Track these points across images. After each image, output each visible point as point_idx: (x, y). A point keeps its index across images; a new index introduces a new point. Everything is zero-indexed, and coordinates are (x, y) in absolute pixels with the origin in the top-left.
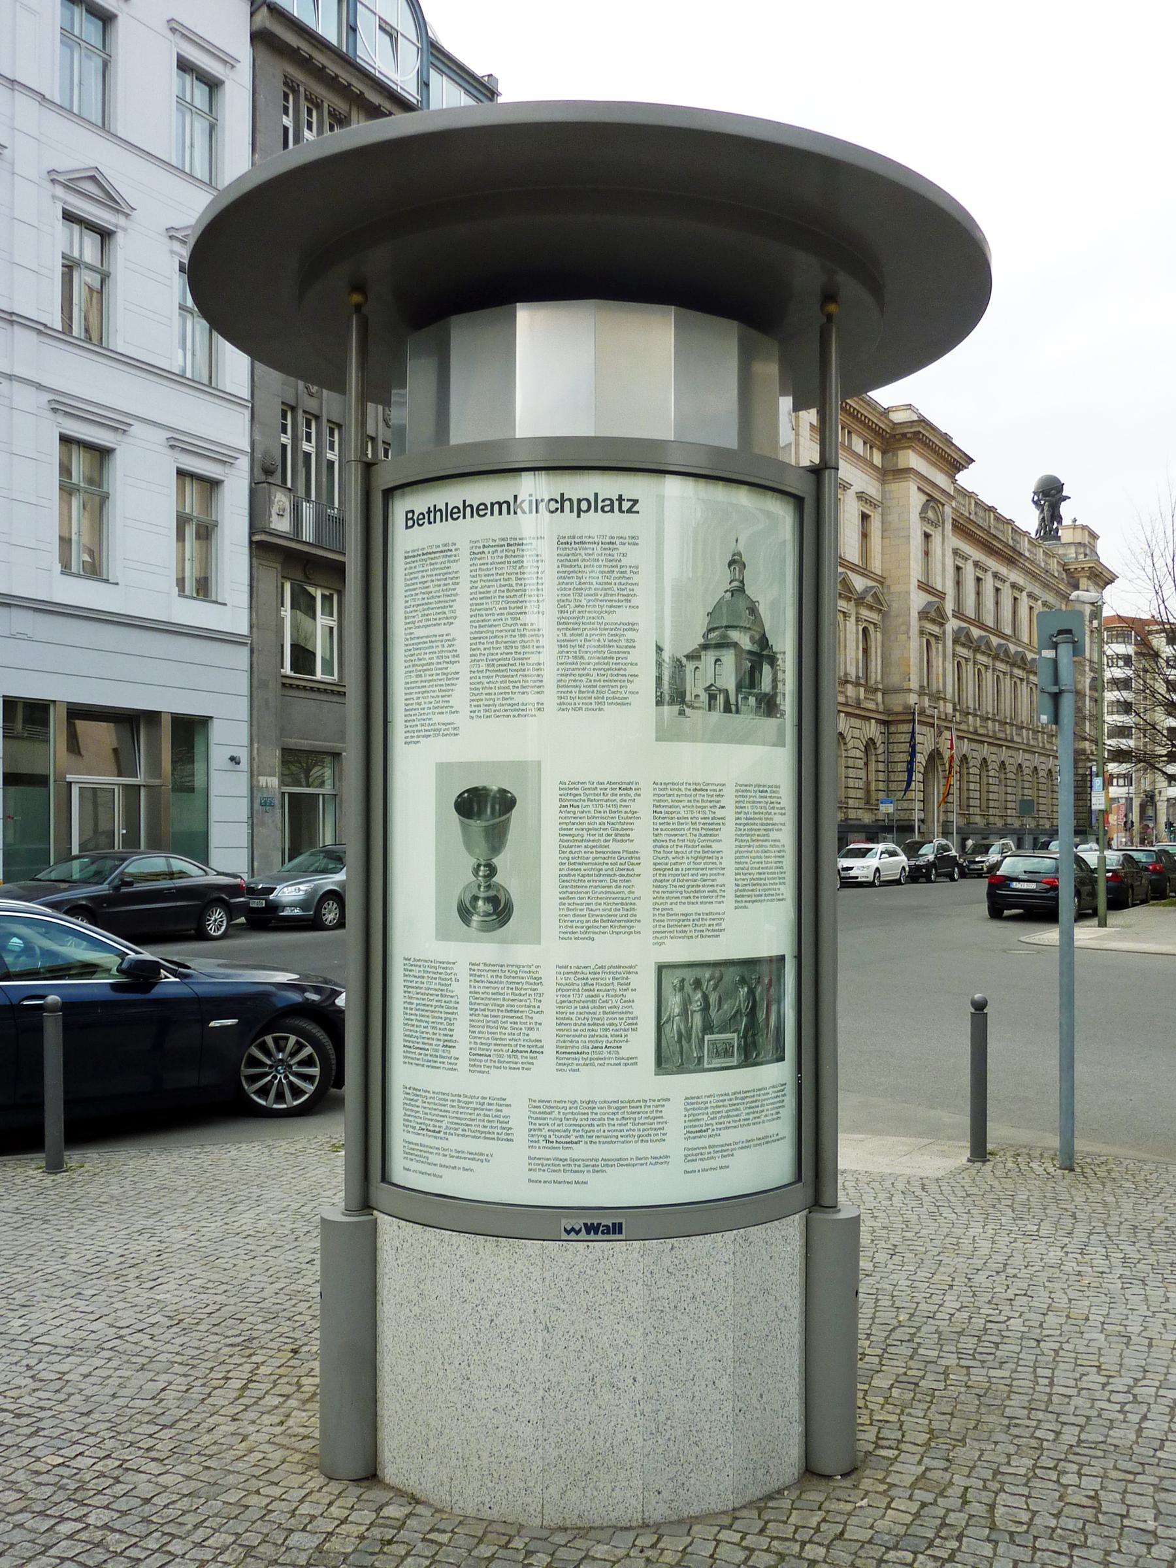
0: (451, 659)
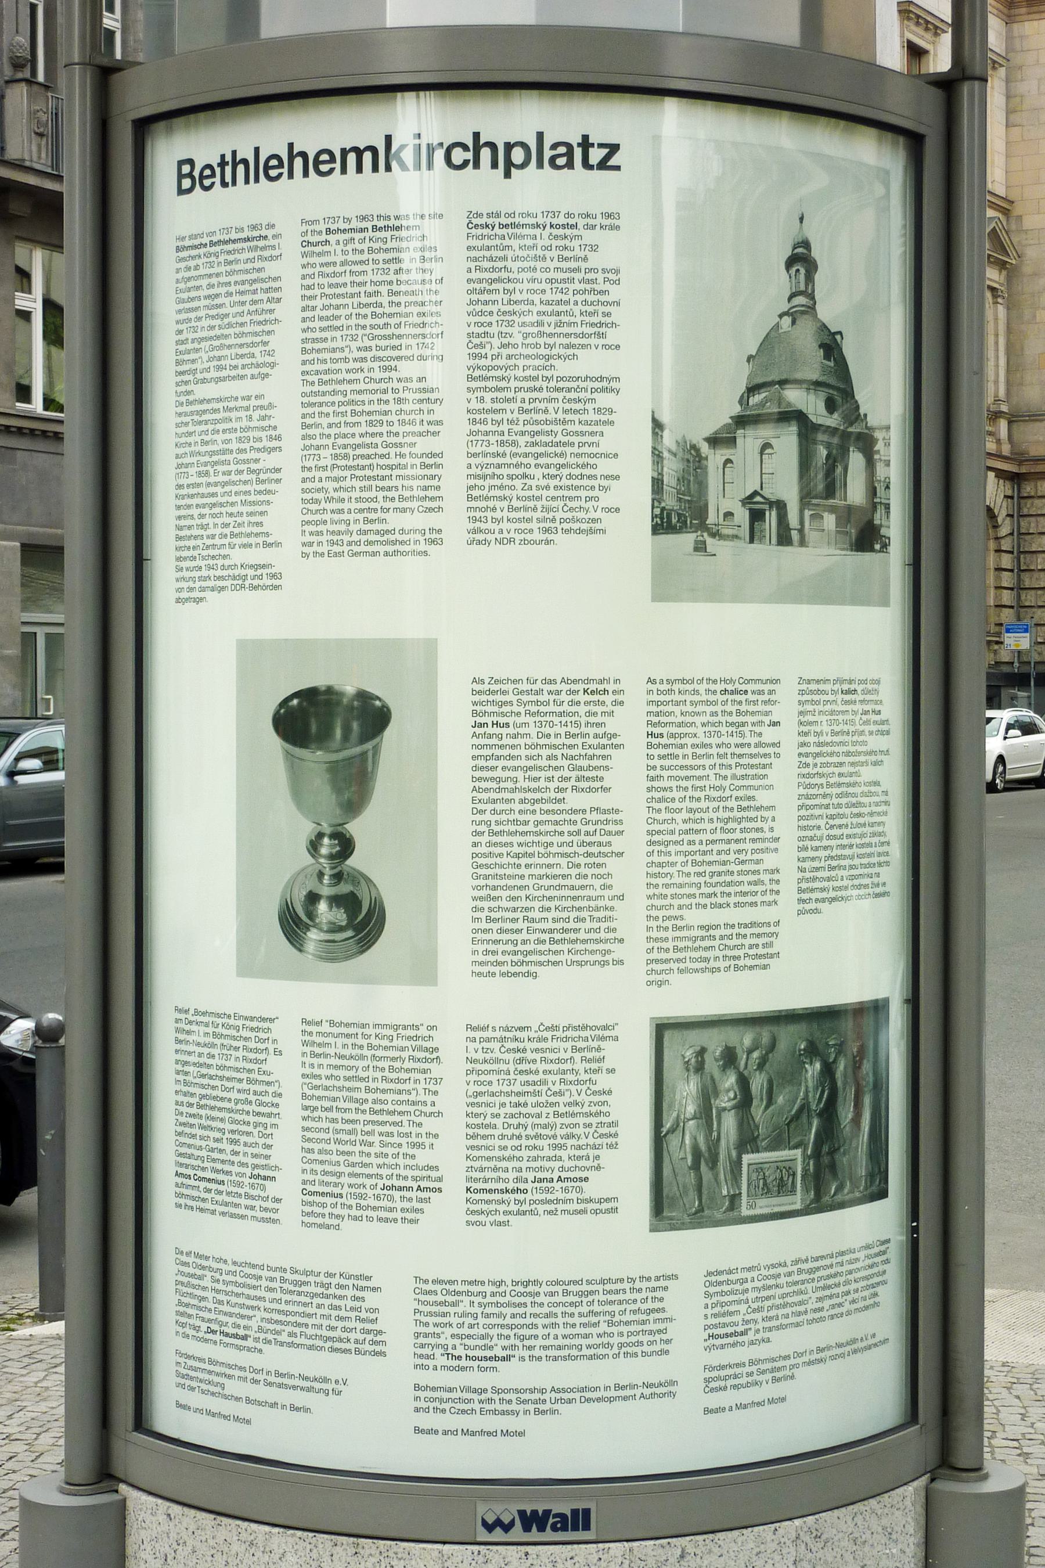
0: (265, 443)
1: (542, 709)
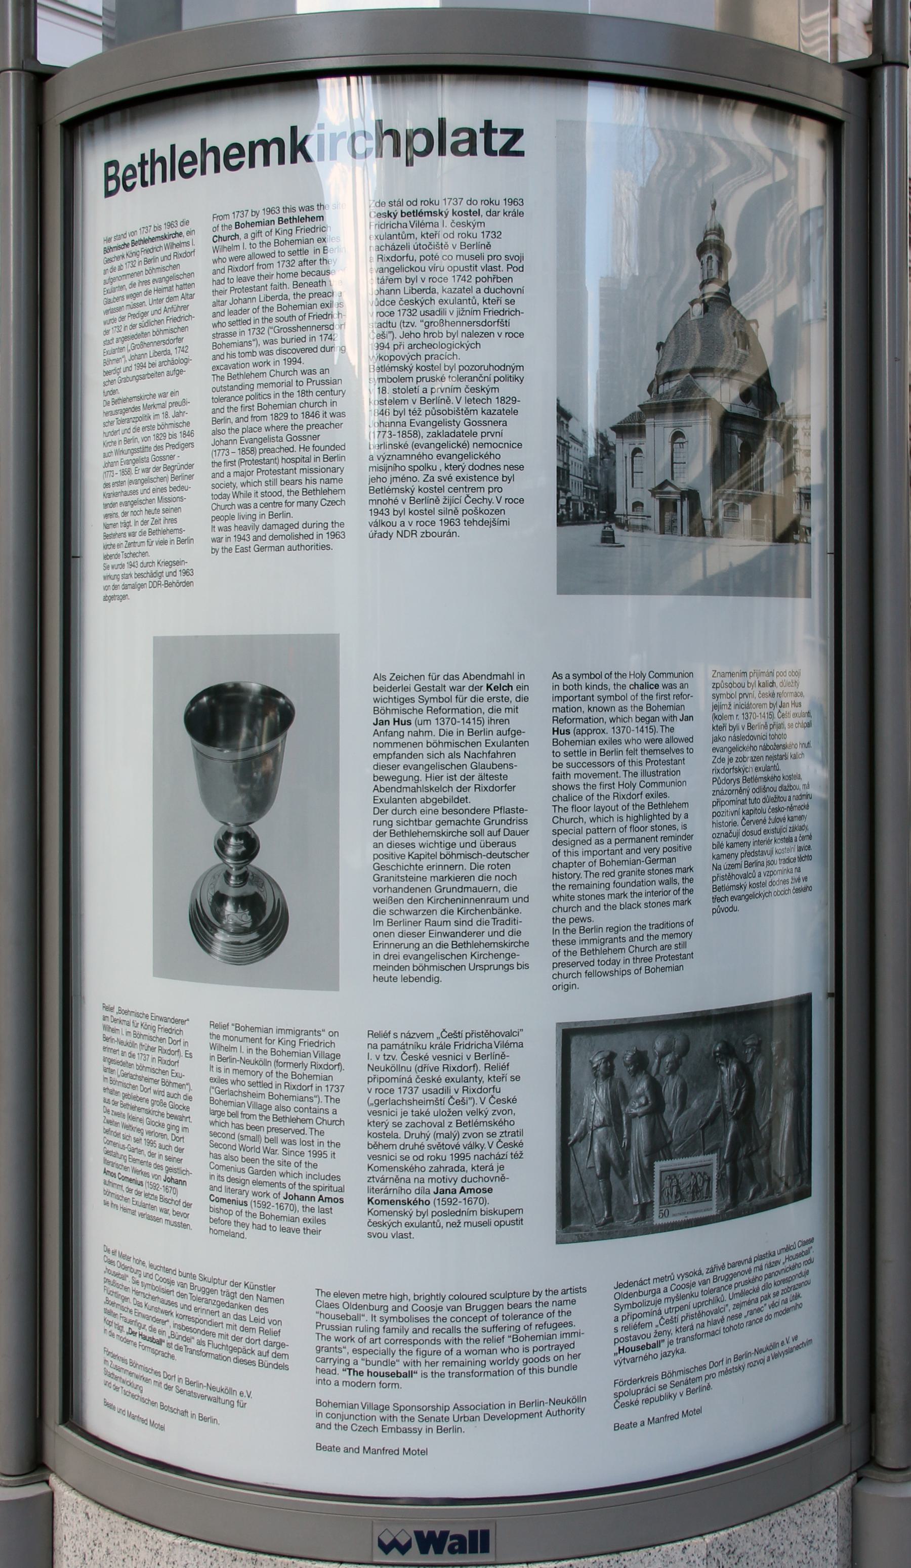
1: (445, 705)
